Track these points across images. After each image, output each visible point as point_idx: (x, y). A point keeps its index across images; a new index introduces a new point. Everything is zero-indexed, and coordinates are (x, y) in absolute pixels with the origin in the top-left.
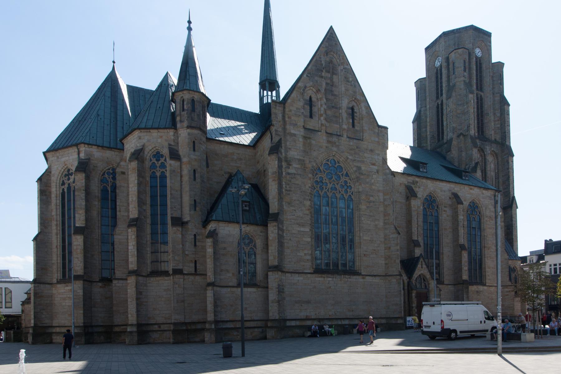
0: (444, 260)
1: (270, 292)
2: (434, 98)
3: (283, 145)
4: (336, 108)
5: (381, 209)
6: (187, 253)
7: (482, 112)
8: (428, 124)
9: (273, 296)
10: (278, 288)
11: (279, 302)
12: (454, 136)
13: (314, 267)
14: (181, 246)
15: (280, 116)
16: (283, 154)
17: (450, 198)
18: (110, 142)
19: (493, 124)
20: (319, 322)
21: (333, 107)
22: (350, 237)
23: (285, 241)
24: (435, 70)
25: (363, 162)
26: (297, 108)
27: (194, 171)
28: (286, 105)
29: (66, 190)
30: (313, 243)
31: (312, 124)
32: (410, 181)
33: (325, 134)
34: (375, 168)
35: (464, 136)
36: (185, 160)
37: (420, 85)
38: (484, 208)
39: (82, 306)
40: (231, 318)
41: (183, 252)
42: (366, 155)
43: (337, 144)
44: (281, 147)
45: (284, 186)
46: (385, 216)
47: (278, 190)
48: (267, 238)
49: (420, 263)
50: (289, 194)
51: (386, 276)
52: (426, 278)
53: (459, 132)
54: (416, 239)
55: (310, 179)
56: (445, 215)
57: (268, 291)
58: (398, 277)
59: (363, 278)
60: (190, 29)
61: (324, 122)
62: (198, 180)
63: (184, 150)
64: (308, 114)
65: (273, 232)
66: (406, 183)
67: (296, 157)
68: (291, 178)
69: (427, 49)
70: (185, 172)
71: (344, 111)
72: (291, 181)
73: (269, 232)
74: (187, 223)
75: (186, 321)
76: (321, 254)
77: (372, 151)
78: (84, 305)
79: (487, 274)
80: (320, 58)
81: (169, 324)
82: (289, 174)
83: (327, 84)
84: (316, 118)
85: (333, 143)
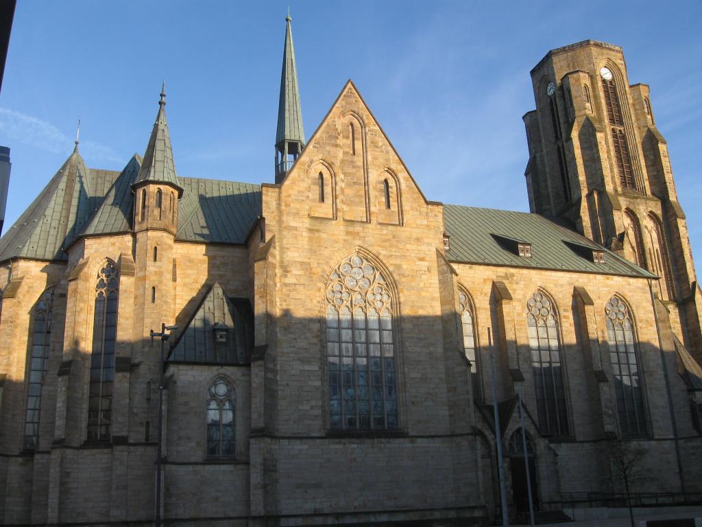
0: (573, 400)
1: (252, 470)
2: (552, 138)
3: (277, 244)
6: (135, 411)
13: (328, 427)
14: (128, 400)
15: (274, 204)
16: (278, 257)
20: (337, 518)
21: (355, 183)
23: (279, 388)
24: (549, 100)
25: (404, 257)
26: (299, 192)
27: (154, 288)
32: (500, 274)
37: (529, 118)
42: (408, 246)
43: (362, 234)
44: (275, 248)
45: (278, 304)
46: (445, 337)
48: (250, 386)
49: (516, 409)
54: (516, 367)
57: (249, 469)
58: (471, 437)
59: (412, 442)
65: (257, 376)
68: (290, 291)
69: (533, 72)
72: (288, 296)
74: (138, 365)
75: (129, 520)
76: (340, 405)
77: (418, 239)
80: (334, 121)
82: (286, 285)
83: (345, 153)
85: (354, 235)
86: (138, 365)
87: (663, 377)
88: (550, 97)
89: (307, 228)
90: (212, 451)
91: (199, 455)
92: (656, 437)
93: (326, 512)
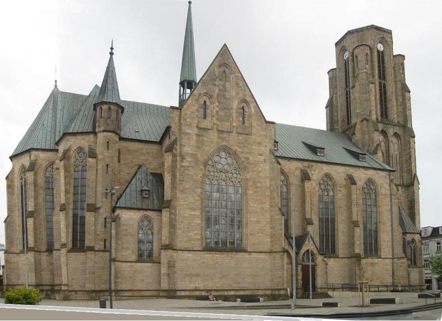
1: (162, 266)
3: (178, 143)
4: (228, 109)
5: (268, 193)
6: (98, 233)
7: (385, 98)
8: (339, 109)
9: (164, 270)
10: (168, 263)
11: (168, 275)
12: (359, 121)
13: (204, 245)
14: (94, 228)
16: (178, 150)
17: (345, 179)
18: (50, 145)
19: (395, 108)
21: (224, 108)
22: (239, 219)
25: (251, 153)
26: (192, 112)
27: (107, 165)
28: (183, 109)
29: (23, 184)
30: (203, 225)
31: (206, 124)
33: (216, 131)
34: (262, 158)
35: (367, 120)
36: (100, 157)
38: (379, 187)
39: (34, 270)
40: (130, 288)
41: (95, 232)
43: (227, 139)
44: (177, 145)
45: (178, 177)
46: (271, 199)
47: (171, 180)
49: (307, 240)
50: (182, 184)
51: (270, 252)
52: (313, 253)
53: (363, 117)
55: (202, 170)
56: (340, 195)
59: (249, 255)
60: (111, 54)
61: (215, 121)
62: (110, 173)
63: (100, 150)
64: (202, 116)
65: (165, 216)
66: (302, 167)
67: (189, 152)
69: (337, 44)
70: (100, 167)
71: (234, 111)
72: (184, 173)
73: (163, 216)
74: (99, 208)
75: (96, 290)
77: (259, 143)
78: (35, 269)
79: (382, 247)
81: (83, 291)
82: (183, 166)
83: (220, 90)
84: (209, 118)
85: (223, 139)
86: (99, 208)
87: (390, 225)
88: (345, 60)
89: (196, 134)
90: (140, 256)
91: (134, 257)
92: (382, 257)
93: (201, 289)
